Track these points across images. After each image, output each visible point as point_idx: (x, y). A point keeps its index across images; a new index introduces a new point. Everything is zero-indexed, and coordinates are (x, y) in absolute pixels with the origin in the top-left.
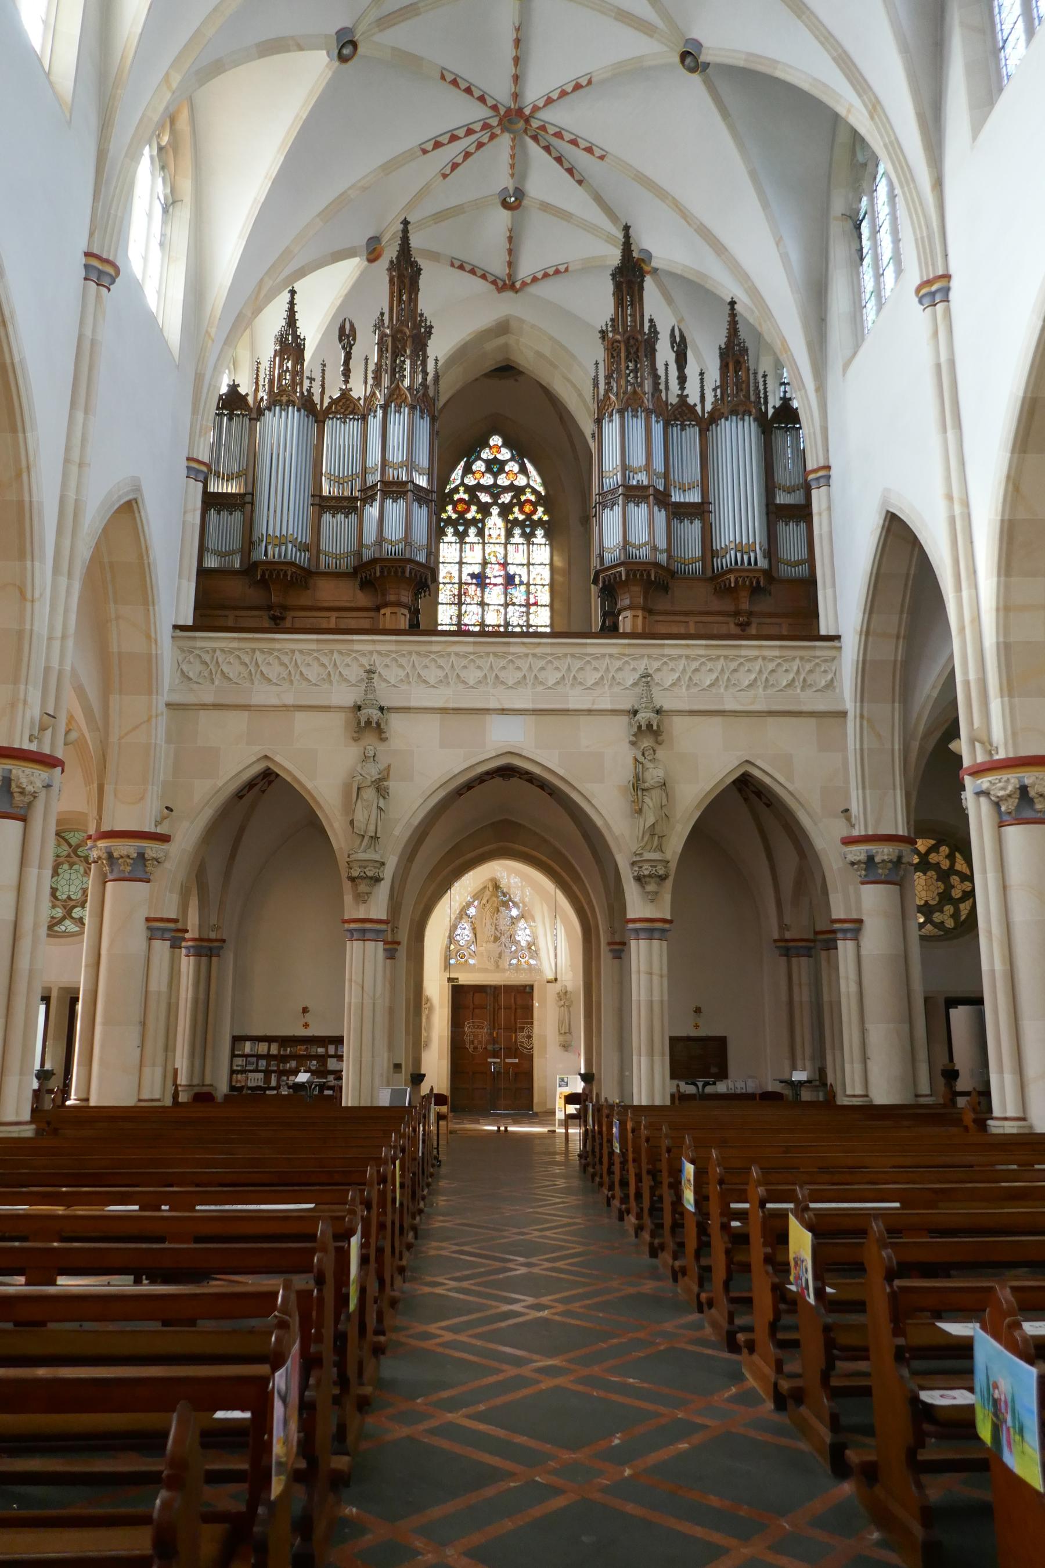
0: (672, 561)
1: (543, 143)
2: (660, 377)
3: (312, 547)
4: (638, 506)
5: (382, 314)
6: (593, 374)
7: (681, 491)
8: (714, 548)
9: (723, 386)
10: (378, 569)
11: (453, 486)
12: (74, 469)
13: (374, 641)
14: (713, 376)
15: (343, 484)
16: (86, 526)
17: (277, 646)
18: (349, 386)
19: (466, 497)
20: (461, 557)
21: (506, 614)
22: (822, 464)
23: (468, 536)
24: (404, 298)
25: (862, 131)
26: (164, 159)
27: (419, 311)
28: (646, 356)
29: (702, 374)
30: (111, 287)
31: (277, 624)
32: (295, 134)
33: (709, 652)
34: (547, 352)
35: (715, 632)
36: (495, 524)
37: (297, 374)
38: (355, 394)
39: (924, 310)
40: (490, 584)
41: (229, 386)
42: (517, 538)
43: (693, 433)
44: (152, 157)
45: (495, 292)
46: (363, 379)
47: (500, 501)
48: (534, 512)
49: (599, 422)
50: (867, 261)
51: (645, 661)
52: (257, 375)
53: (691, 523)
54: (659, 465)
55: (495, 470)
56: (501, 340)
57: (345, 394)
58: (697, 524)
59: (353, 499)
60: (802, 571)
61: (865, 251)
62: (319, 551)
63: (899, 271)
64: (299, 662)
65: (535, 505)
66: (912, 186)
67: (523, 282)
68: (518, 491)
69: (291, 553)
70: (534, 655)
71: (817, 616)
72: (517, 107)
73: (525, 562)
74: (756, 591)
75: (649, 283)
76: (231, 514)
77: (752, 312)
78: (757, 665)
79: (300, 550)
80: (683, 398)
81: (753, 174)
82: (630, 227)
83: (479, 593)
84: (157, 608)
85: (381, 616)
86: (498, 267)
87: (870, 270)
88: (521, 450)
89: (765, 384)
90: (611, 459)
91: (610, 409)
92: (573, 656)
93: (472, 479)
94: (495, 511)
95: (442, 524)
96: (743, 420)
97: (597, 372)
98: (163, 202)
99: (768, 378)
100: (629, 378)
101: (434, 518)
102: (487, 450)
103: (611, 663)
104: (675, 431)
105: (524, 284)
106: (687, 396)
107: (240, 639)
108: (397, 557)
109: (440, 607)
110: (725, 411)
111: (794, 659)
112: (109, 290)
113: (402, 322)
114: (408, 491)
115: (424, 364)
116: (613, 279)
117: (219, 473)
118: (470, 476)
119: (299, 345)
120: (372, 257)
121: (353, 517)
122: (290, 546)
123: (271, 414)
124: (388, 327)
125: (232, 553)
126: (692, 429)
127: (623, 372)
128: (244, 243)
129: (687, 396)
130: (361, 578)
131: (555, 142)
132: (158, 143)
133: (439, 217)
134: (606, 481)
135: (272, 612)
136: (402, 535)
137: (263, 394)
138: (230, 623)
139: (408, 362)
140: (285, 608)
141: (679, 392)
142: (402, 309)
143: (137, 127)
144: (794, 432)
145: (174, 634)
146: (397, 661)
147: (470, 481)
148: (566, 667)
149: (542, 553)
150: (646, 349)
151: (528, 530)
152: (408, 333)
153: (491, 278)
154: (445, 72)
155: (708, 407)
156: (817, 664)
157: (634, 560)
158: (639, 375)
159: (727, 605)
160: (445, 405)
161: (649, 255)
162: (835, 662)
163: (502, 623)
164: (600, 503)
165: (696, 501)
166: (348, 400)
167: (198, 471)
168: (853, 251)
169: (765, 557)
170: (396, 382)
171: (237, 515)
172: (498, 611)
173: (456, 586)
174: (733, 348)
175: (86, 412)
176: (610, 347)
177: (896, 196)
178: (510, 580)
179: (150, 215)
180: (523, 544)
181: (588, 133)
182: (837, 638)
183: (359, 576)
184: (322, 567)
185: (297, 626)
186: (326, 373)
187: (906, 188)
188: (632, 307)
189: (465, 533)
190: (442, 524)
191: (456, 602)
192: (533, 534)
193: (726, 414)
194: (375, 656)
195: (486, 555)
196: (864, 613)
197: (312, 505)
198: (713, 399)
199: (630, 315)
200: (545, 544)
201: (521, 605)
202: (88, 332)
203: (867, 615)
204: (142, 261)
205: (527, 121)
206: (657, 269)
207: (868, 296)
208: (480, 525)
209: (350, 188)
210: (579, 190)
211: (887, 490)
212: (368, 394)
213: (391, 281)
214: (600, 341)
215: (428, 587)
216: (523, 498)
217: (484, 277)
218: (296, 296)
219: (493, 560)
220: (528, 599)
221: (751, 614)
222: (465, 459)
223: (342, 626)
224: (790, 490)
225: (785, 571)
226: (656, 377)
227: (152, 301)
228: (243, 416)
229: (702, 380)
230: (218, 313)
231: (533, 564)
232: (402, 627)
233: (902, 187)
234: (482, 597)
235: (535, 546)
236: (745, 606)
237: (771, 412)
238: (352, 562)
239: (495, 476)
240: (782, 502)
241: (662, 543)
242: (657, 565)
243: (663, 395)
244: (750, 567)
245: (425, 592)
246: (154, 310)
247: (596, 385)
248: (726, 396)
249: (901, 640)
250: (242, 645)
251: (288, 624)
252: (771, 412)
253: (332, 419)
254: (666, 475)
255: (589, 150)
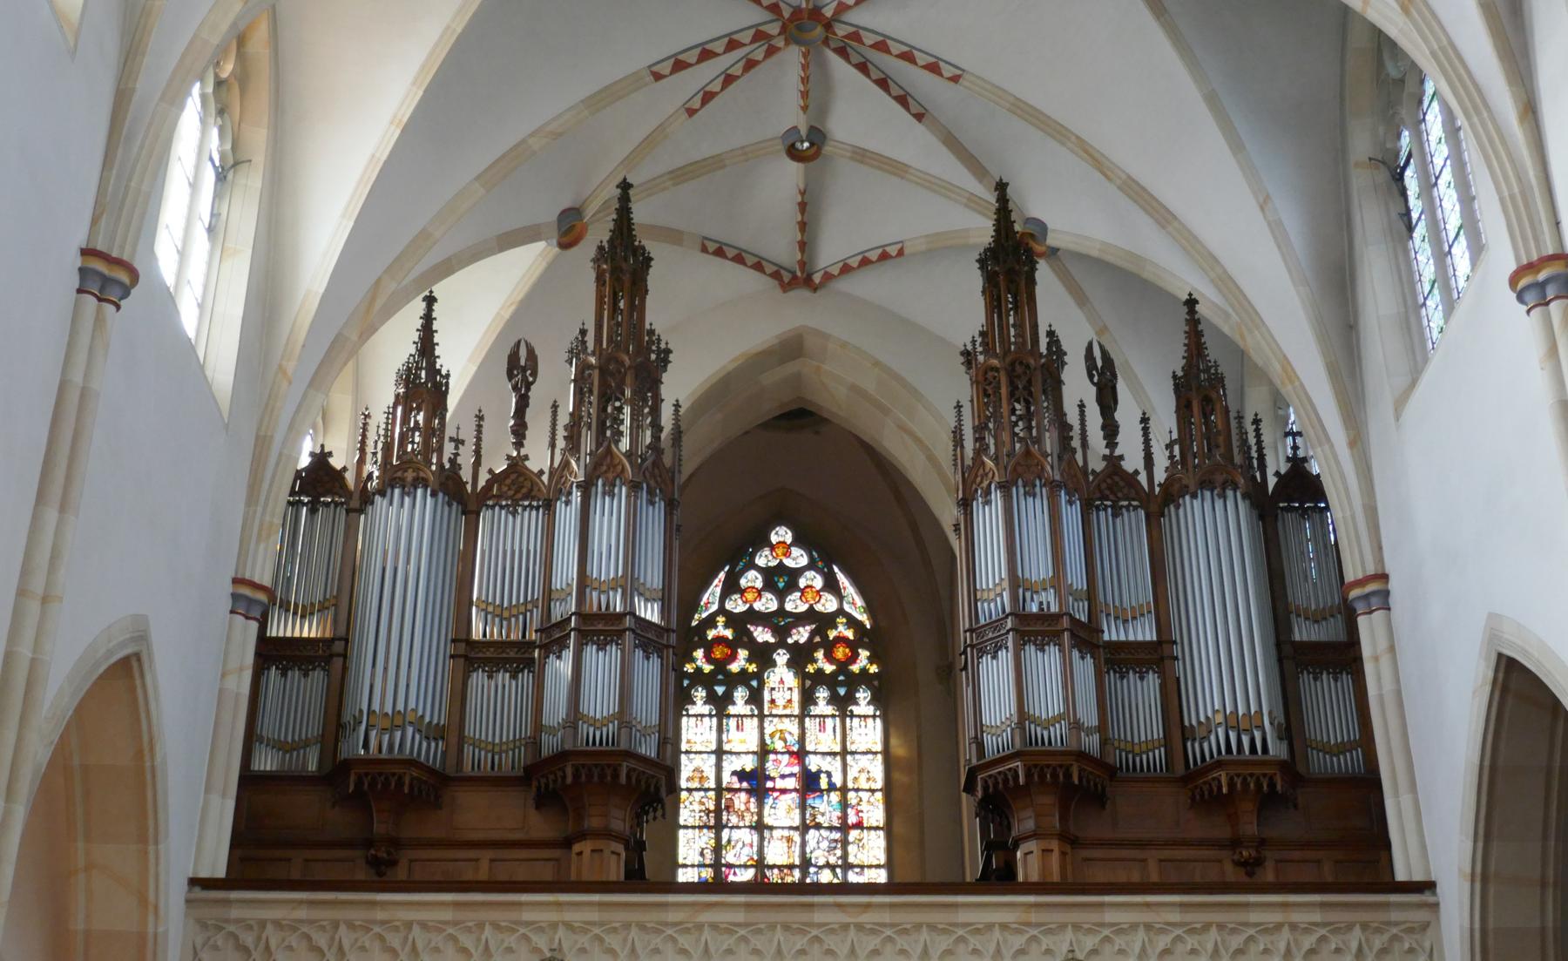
0: (1109, 748)
1: (856, 59)
2: (1071, 428)
3: (451, 731)
4: (1043, 651)
5: (583, 332)
6: (953, 424)
7: (1120, 623)
8: (1187, 723)
9: (1184, 439)
10: (569, 771)
11: (704, 615)
12: (34, 607)
13: (558, 904)
14: (1166, 424)
15: (509, 620)
16: (47, 705)
17: (380, 915)
18: (523, 452)
19: (729, 633)
20: (720, 742)
21: (804, 844)
22: (1371, 570)
23: (734, 703)
24: (622, 305)
25: (1392, 31)
26: (221, 105)
27: (647, 326)
28: (1044, 392)
29: (1145, 420)
30: (123, 303)
31: (380, 874)
32: (443, 56)
33: (1190, 917)
34: (869, 386)
35: (1198, 879)
36: (782, 682)
37: (433, 433)
38: (533, 465)
39: (1528, 312)
40: (774, 789)
41: (312, 454)
42: (822, 707)
43: (1135, 521)
44: (203, 97)
45: (778, 290)
46: (547, 440)
47: (790, 641)
48: (854, 658)
49: (966, 504)
50: (1420, 231)
51: (1069, 935)
52: (364, 436)
53: (1142, 678)
54: (1076, 577)
55: (781, 585)
56: (791, 368)
57: (516, 466)
58: (1153, 680)
59: (528, 646)
60: (1349, 762)
61: (1415, 215)
62: (462, 739)
63: (1477, 249)
64: (420, 945)
65: (854, 646)
66: (1485, 115)
67: (826, 273)
68: (824, 622)
69: (411, 743)
70: (860, 927)
71: (1387, 845)
72: (811, 6)
73: (837, 749)
74: (1270, 801)
75: (1044, 275)
76: (306, 675)
77: (1227, 316)
78: (1282, 940)
79: (427, 738)
80: (1113, 461)
81: (1212, 100)
82: (1007, 184)
83: (753, 807)
84: (161, 847)
85: (574, 856)
86: (783, 250)
87: (1426, 245)
88: (825, 554)
89: (1258, 435)
90: (991, 568)
91: (985, 483)
92: (932, 927)
93: (740, 602)
94: (781, 657)
95: (686, 683)
96: (1224, 497)
97: (960, 420)
98: (217, 164)
99: (1263, 425)
100: (1017, 430)
101: (672, 675)
102: (767, 552)
103: (1005, 941)
104: (1103, 518)
105: (828, 277)
106: (1121, 457)
107: (311, 903)
108: (604, 748)
109: (681, 833)
110: (1190, 481)
111: (1350, 927)
112: (118, 307)
113: (618, 345)
114: (624, 631)
115: (656, 411)
116: (981, 268)
117: (289, 603)
118: (737, 596)
119: (437, 386)
120: (565, 240)
121: (526, 678)
122: (410, 730)
123: (386, 502)
124: (593, 354)
125: (306, 744)
126: (1132, 513)
127: (1005, 420)
128: (351, 224)
129: (1121, 457)
130: (539, 788)
131: (876, 57)
132: (216, 75)
133: (681, 175)
134: (983, 607)
135: (373, 852)
136: (613, 707)
137: (371, 468)
138: (296, 875)
139: (627, 410)
140: (395, 843)
141: (1107, 452)
142: (618, 324)
143: (184, 56)
144: (1316, 516)
145: (192, 896)
146: (601, 940)
147: (736, 605)
148: (919, 949)
149: (868, 733)
150: (1044, 382)
151: (842, 691)
152: (627, 362)
153: (770, 269)
154: (706, 242)
155: (1160, 476)
156: (1395, 938)
157: (1040, 748)
158: (1034, 424)
159: (1220, 829)
160: (691, 476)
161: (1042, 226)
162: (1429, 932)
163: (797, 862)
164: (972, 646)
165: (1148, 638)
166: (521, 474)
167: (251, 602)
168: (1394, 215)
169: (1280, 739)
170: (605, 444)
171: (318, 676)
172: (789, 840)
173: (712, 794)
174: (1198, 376)
175: (63, 508)
176: (981, 378)
177: (1460, 128)
178: (809, 783)
179: (194, 186)
180: (833, 716)
181: (929, 41)
182: (1429, 886)
183: (535, 783)
184: (467, 768)
185: (417, 877)
186: (484, 430)
187: (1475, 119)
188: (1016, 313)
189: (728, 699)
190: (686, 683)
191: (712, 822)
192: (851, 699)
193: (1192, 488)
194: (561, 932)
195: (767, 738)
196: (1475, 841)
197: (452, 656)
198: (1167, 463)
199: (1014, 326)
200: (874, 717)
201: (831, 828)
202: (77, 377)
203: (1480, 844)
204: (176, 257)
205: (828, 26)
206: (1058, 250)
207: (1427, 288)
208: (754, 683)
209: (532, 135)
210: (919, 128)
211: (1493, 618)
212: (556, 465)
213: (600, 280)
214: (963, 368)
215: (660, 801)
216: (832, 634)
217: (758, 267)
218: (435, 307)
219: (779, 746)
220: (844, 817)
221: (1262, 843)
222: (727, 568)
223: (502, 877)
224: (1317, 618)
225: (1319, 763)
226: (1064, 428)
227: (189, 319)
228: (337, 504)
229: (1146, 431)
230: (302, 336)
231: (853, 753)
232: (613, 878)
233: (1468, 117)
234: (760, 814)
235: (856, 720)
236: (1250, 827)
237: (1272, 481)
238: (522, 757)
239: (781, 596)
240: (1305, 638)
241: (1088, 714)
242: (1081, 755)
243: (1079, 457)
244: (1254, 757)
245: (655, 810)
246: (191, 334)
247: (958, 440)
248: (1190, 458)
249: (1550, 891)
250: (317, 914)
251: (401, 873)
252: (1272, 481)
253: (493, 507)
254: (1091, 594)
255: (933, 68)
